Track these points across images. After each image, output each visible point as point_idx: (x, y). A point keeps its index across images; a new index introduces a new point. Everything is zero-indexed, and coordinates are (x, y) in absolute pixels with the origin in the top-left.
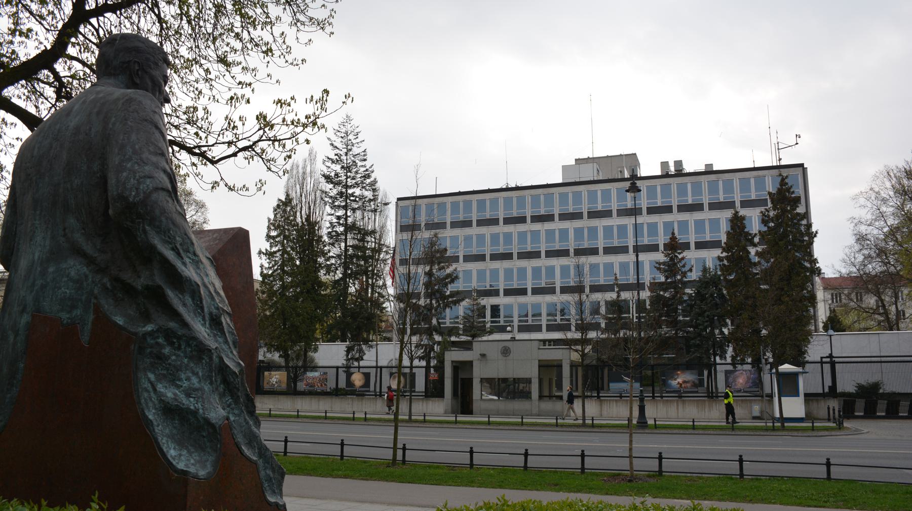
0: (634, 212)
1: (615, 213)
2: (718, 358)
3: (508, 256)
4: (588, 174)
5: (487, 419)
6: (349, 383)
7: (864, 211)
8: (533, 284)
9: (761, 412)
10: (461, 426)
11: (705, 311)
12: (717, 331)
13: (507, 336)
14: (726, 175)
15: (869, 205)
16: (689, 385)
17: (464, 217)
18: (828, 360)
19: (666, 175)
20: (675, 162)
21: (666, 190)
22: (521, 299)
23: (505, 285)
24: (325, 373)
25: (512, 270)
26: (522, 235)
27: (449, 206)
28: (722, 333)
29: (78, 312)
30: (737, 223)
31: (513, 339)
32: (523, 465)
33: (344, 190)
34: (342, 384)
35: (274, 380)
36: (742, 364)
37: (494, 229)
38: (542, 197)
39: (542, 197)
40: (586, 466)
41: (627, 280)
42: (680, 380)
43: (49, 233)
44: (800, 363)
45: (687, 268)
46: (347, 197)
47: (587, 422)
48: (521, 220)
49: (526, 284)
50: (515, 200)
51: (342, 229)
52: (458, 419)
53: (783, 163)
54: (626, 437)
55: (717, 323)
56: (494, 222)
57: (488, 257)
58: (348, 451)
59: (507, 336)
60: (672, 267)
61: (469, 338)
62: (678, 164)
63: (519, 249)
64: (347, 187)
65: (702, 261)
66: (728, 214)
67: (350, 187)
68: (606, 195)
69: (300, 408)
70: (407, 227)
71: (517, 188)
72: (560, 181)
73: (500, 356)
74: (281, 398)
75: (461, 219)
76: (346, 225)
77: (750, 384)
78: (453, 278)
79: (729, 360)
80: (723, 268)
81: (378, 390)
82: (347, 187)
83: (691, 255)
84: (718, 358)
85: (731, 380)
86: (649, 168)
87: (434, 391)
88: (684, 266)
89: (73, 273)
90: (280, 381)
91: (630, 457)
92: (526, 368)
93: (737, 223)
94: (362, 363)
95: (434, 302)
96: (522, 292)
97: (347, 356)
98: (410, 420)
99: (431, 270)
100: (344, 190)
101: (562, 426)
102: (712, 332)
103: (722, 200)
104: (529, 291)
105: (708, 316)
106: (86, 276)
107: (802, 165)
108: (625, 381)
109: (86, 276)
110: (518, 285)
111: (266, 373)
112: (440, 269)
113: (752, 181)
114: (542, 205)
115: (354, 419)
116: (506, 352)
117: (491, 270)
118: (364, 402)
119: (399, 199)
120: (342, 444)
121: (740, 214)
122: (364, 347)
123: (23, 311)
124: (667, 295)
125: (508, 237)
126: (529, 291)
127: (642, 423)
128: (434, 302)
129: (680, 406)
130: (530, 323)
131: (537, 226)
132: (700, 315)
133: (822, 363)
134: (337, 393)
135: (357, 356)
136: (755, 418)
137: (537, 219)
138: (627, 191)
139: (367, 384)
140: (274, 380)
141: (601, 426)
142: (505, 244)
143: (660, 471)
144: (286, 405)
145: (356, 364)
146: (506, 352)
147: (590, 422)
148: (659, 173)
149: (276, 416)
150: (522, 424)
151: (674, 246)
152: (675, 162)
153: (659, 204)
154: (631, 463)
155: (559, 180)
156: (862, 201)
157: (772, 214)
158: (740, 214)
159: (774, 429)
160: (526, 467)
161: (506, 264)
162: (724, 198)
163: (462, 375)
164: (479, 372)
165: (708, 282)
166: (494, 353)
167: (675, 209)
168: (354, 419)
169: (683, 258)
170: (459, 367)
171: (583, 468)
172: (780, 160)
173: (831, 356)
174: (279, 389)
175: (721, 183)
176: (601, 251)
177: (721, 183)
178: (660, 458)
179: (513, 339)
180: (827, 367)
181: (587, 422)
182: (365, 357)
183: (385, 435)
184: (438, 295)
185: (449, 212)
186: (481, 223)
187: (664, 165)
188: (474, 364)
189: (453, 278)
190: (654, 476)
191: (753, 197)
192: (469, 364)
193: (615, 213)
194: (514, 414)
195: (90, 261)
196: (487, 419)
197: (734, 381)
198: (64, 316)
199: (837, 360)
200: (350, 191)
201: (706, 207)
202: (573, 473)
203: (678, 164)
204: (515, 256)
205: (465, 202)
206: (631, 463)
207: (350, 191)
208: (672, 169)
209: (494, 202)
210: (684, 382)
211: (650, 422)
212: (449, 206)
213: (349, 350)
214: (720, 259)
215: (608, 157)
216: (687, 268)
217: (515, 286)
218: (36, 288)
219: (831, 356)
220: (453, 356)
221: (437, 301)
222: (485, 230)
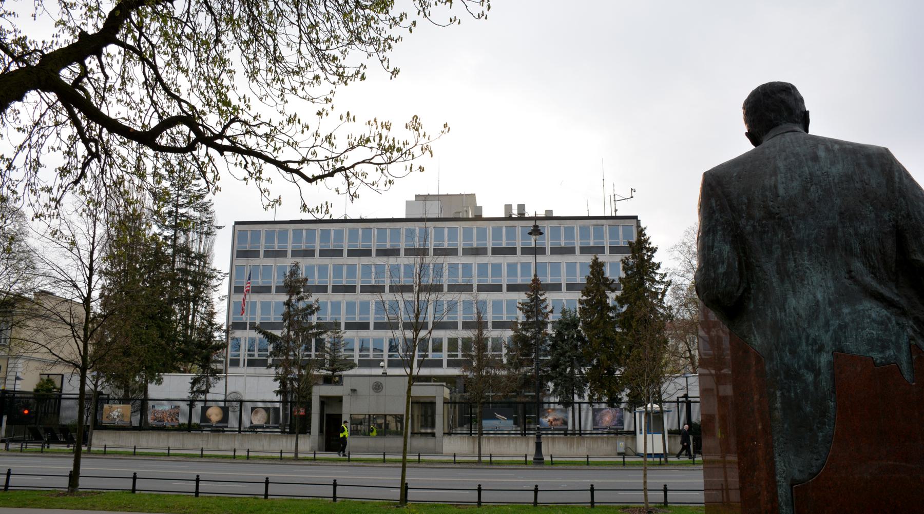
0: (537, 251)
1: (460, 251)
2: (576, 396)
3: (351, 289)
4: (433, 211)
5: (417, 458)
6: (204, 417)
7: (678, 263)
8: (376, 318)
9: (626, 448)
10: (423, 465)
11: (566, 352)
12: (576, 371)
13: (379, 371)
14: (568, 221)
15: (682, 258)
16: (559, 423)
17: (334, 246)
18: (684, 399)
19: (509, 218)
20: (519, 206)
21: (511, 232)
22: (363, 333)
23: (347, 318)
24: (177, 407)
25: (355, 303)
26: (367, 268)
27: (263, 234)
28: (581, 372)
29: (890, 352)
30: (597, 267)
31: (385, 375)
32: (533, 501)
33: (174, 209)
34: (196, 419)
35: (115, 414)
36: (599, 403)
37: (337, 261)
38: (388, 231)
39: (388, 231)
40: (482, 500)
41: (471, 318)
42: (550, 418)
43: (829, 275)
44: (660, 402)
45: (548, 309)
46: (176, 217)
47: (483, 459)
48: (366, 253)
49: (368, 318)
50: (360, 232)
51: (170, 251)
52: (317, 456)
53: (619, 214)
54: (641, 474)
55: (575, 362)
56: (338, 253)
57: (330, 289)
58: (340, 492)
59: (379, 371)
60: (534, 308)
61: (330, 373)
62: (521, 207)
63: (362, 282)
64: (177, 206)
65: (564, 302)
66: (588, 259)
67: (181, 206)
68: (453, 233)
69: (204, 447)
70: (241, 253)
71: (346, 221)
72: (403, 216)
73: (372, 392)
74: (123, 433)
75: (304, 248)
76: (174, 246)
77: (615, 422)
78: (310, 310)
79: (587, 399)
80: (583, 311)
81: (577, 427)
82: (177, 206)
83: (550, 298)
84: (576, 396)
85: (598, 418)
86: (492, 209)
87: (299, 427)
88: (546, 307)
89: (874, 315)
90: (123, 415)
91: (645, 490)
92: (394, 403)
93: (597, 267)
94: (209, 396)
95: (292, 333)
96: (364, 326)
97: (192, 388)
98: (296, 458)
99: (290, 300)
100: (174, 209)
101: (460, 463)
102: (572, 371)
103: (563, 245)
104: (372, 326)
105: (569, 357)
106: (889, 319)
107: (636, 217)
108: (498, 419)
109: (889, 319)
110: (360, 318)
111: (106, 406)
112: (299, 300)
113: (592, 229)
114: (360, 240)
115: (234, 457)
116: (378, 387)
117: (332, 303)
118: (221, 438)
119: (237, 223)
120: (335, 485)
121: (599, 260)
122: (211, 379)
123: (821, 349)
124: (529, 334)
125: (352, 269)
126: (372, 326)
127: (539, 459)
128: (292, 333)
129: (551, 444)
130: (371, 358)
131: (382, 260)
132: (561, 355)
133: (678, 402)
134: (189, 428)
135: (204, 388)
136: (619, 454)
137: (382, 252)
138: (530, 234)
139: (225, 419)
140: (115, 414)
141: (498, 463)
142: (320, 276)
143: (666, 503)
144: (127, 441)
145: (203, 397)
146: (378, 387)
147: (488, 459)
148: (503, 216)
149: (141, 454)
150: (384, 461)
151: (536, 288)
152: (519, 206)
153: (504, 246)
154: (646, 495)
155: (403, 215)
156: (676, 254)
157: (631, 261)
158: (599, 260)
159: (660, 464)
160: (536, 503)
161: (349, 297)
162: (565, 243)
163: (328, 411)
164: (348, 410)
165: (567, 324)
166: (365, 388)
167: (519, 251)
168: (234, 457)
169: (544, 300)
170: (325, 401)
171: (592, 502)
172: (616, 211)
173: (686, 396)
174: (121, 423)
175: (562, 229)
176: (504, 288)
177: (562, 229)
178: (592, 490)
179: (385, 375)
180: (683, 407)
181: (483, 459)
182: (210, 390)
183: (393, 476)
184: (296, 326)
185: (290, 240)
186: (323, 253)
187: (508, 207)
188: (344, 399)
189: (310, 310)
190: (661, 507)
191: (592, 244)
192: (339, 400)
193: (460, 251)
194: (375, 452)
195: (888, 303)
196: (382, 457)
197: (601, 418)
198: (876, 356)
199: (692, 400)
200: (181, 211)
201: (578, 250)
202: (527, 507)
203: (521, 207)
204: (358, 289)
205: (308, 230)
206: (646, 495)
207: (181, 211)
208: (515, 212)
209: (311, 234)
210: (555, 420)
211: (547, 458)
212: (263, 234)
213: (195, 382)
214: (581, 302)
215: (448, 195)
216: (548, 309)
217: (357, 320)
218: (832, 328)
219: (686, 396)
220: (320, 391)
221: (296, 333)
222: (328, 261)
